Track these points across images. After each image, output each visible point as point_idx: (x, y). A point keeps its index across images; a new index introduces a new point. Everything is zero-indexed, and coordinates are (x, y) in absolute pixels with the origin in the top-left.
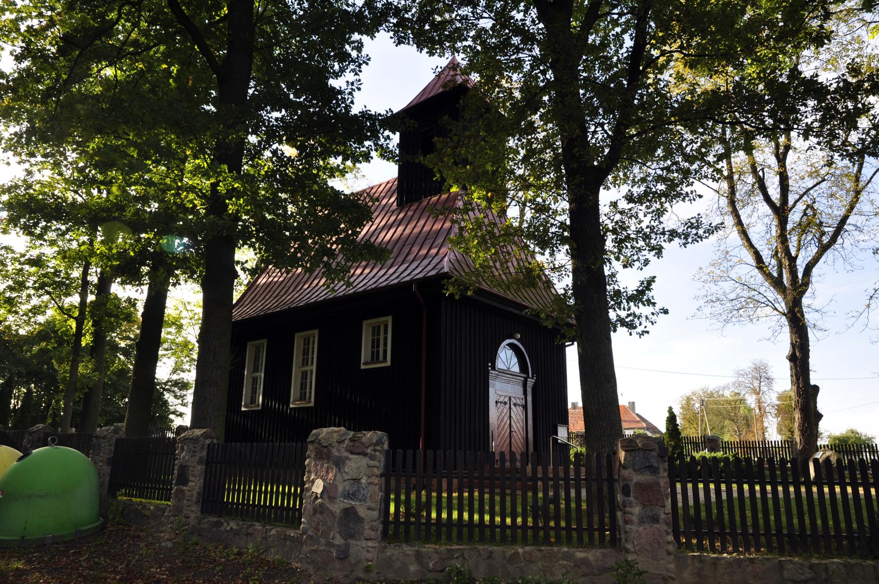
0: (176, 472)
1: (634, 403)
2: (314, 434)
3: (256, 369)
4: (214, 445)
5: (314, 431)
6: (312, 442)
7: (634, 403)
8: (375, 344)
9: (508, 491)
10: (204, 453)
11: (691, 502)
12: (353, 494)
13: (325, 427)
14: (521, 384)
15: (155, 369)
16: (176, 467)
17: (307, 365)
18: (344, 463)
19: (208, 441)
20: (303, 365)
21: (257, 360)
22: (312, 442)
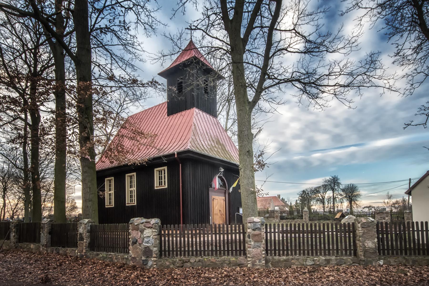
0: (78, 236)
1: (280, 195)
2: (132, 220)
3: (110, 190)
4: (93, 225)
5: (132, 219)
6: (131, 224)
7: (280, 195)
8: (160, 178)
9: (398, 232)
10: (89, 228)
11: (273, 238)
12: (148, 242)
13: (136, 217)
14: (224, 193)
15: (82, 207)
16: (78, 234)
17: (132, 188)
18: (144, 231)
19: (90, 224)
20: (130, 188)
21: (110, 186)
22: (131, 224)
